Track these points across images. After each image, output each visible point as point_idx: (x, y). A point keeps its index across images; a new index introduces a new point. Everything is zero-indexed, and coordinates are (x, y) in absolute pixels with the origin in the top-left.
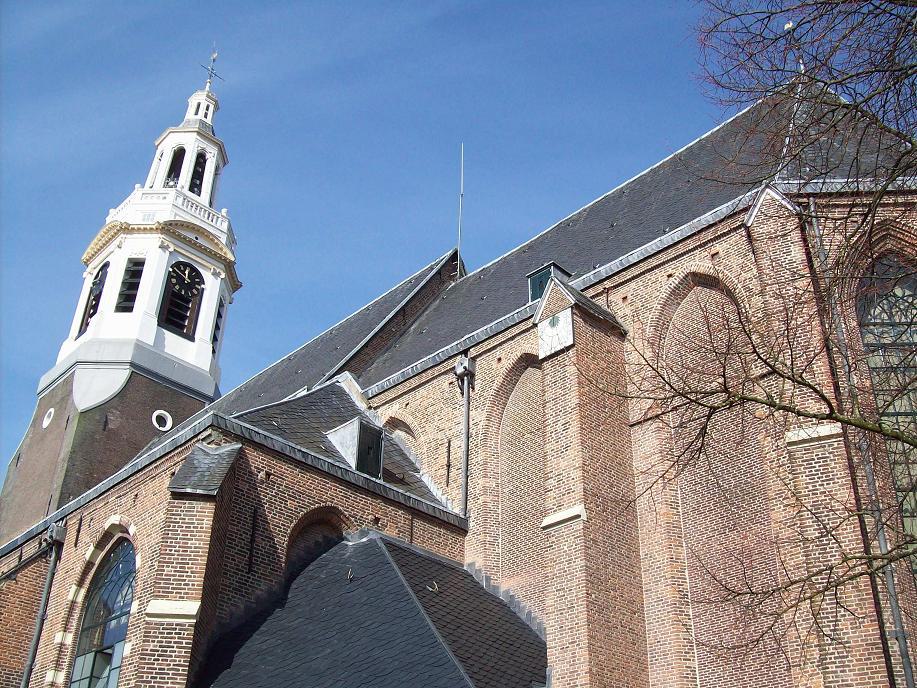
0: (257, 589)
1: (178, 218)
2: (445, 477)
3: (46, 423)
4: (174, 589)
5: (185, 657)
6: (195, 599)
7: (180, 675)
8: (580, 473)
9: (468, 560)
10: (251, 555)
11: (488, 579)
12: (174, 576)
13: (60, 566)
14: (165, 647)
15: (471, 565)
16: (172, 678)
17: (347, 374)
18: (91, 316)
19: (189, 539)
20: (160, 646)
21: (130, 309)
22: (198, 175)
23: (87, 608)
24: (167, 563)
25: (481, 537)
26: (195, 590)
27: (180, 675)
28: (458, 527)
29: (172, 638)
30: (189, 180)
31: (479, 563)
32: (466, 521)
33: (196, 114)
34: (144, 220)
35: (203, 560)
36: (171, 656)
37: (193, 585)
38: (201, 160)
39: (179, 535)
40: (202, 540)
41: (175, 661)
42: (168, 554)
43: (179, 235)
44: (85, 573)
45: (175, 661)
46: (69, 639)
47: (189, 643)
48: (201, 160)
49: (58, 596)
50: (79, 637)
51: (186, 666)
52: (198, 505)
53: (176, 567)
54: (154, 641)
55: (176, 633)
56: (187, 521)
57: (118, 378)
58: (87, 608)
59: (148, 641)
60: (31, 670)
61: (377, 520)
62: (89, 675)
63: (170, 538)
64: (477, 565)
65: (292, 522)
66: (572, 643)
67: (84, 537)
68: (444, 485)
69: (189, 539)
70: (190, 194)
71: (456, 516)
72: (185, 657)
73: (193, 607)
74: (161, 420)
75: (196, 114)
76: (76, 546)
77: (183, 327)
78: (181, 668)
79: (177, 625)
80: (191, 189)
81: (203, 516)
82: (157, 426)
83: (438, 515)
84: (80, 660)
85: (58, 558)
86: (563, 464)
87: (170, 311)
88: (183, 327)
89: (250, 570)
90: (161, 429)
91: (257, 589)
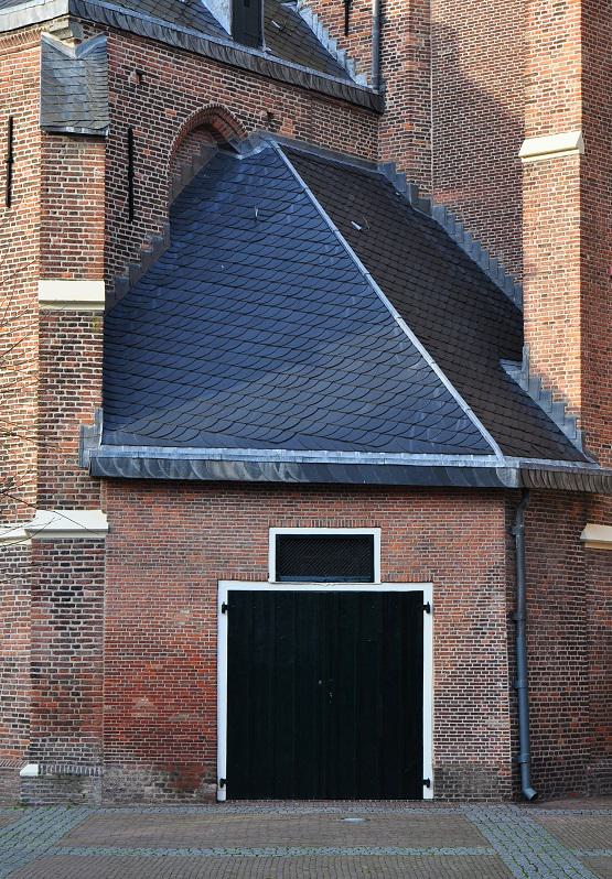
2: (341, 19)
4: (65, 264)
5: (97, 354)
7: (94, 377)
8: (578, 85)
9: (384, 159)
10: (131, 196)
11: (416, 190)
12: (64, 247)
15: (391, 166)
16: (84, 382)
19: (76, 197)
20: (63, 342)
24: (52, 230)
25: (405, 126)
26: (96, 265)
27: (94, 377)
28: (370, 107)
29: (77, 331)
31: (402, 164)
32: (381, 98)
37: (92, 259)
40: (94, 197)
41: (85, 360)
42: (52, 218)
45: (85, 360)
51: (99, 366)
52: (84, 149)
54: (54, 336)
55: (81, 325)
56: (69, 170)
59: (46, 336)
63: (51, 196)
64: (399, 167)
66: (559, 318)
69: (76, 197)
71: (368, 92)
72: (97, 354)
78: (94, 369)
81: (92, 165)
83: (346, 96)
86: (554, 66)
89: (132, 217)
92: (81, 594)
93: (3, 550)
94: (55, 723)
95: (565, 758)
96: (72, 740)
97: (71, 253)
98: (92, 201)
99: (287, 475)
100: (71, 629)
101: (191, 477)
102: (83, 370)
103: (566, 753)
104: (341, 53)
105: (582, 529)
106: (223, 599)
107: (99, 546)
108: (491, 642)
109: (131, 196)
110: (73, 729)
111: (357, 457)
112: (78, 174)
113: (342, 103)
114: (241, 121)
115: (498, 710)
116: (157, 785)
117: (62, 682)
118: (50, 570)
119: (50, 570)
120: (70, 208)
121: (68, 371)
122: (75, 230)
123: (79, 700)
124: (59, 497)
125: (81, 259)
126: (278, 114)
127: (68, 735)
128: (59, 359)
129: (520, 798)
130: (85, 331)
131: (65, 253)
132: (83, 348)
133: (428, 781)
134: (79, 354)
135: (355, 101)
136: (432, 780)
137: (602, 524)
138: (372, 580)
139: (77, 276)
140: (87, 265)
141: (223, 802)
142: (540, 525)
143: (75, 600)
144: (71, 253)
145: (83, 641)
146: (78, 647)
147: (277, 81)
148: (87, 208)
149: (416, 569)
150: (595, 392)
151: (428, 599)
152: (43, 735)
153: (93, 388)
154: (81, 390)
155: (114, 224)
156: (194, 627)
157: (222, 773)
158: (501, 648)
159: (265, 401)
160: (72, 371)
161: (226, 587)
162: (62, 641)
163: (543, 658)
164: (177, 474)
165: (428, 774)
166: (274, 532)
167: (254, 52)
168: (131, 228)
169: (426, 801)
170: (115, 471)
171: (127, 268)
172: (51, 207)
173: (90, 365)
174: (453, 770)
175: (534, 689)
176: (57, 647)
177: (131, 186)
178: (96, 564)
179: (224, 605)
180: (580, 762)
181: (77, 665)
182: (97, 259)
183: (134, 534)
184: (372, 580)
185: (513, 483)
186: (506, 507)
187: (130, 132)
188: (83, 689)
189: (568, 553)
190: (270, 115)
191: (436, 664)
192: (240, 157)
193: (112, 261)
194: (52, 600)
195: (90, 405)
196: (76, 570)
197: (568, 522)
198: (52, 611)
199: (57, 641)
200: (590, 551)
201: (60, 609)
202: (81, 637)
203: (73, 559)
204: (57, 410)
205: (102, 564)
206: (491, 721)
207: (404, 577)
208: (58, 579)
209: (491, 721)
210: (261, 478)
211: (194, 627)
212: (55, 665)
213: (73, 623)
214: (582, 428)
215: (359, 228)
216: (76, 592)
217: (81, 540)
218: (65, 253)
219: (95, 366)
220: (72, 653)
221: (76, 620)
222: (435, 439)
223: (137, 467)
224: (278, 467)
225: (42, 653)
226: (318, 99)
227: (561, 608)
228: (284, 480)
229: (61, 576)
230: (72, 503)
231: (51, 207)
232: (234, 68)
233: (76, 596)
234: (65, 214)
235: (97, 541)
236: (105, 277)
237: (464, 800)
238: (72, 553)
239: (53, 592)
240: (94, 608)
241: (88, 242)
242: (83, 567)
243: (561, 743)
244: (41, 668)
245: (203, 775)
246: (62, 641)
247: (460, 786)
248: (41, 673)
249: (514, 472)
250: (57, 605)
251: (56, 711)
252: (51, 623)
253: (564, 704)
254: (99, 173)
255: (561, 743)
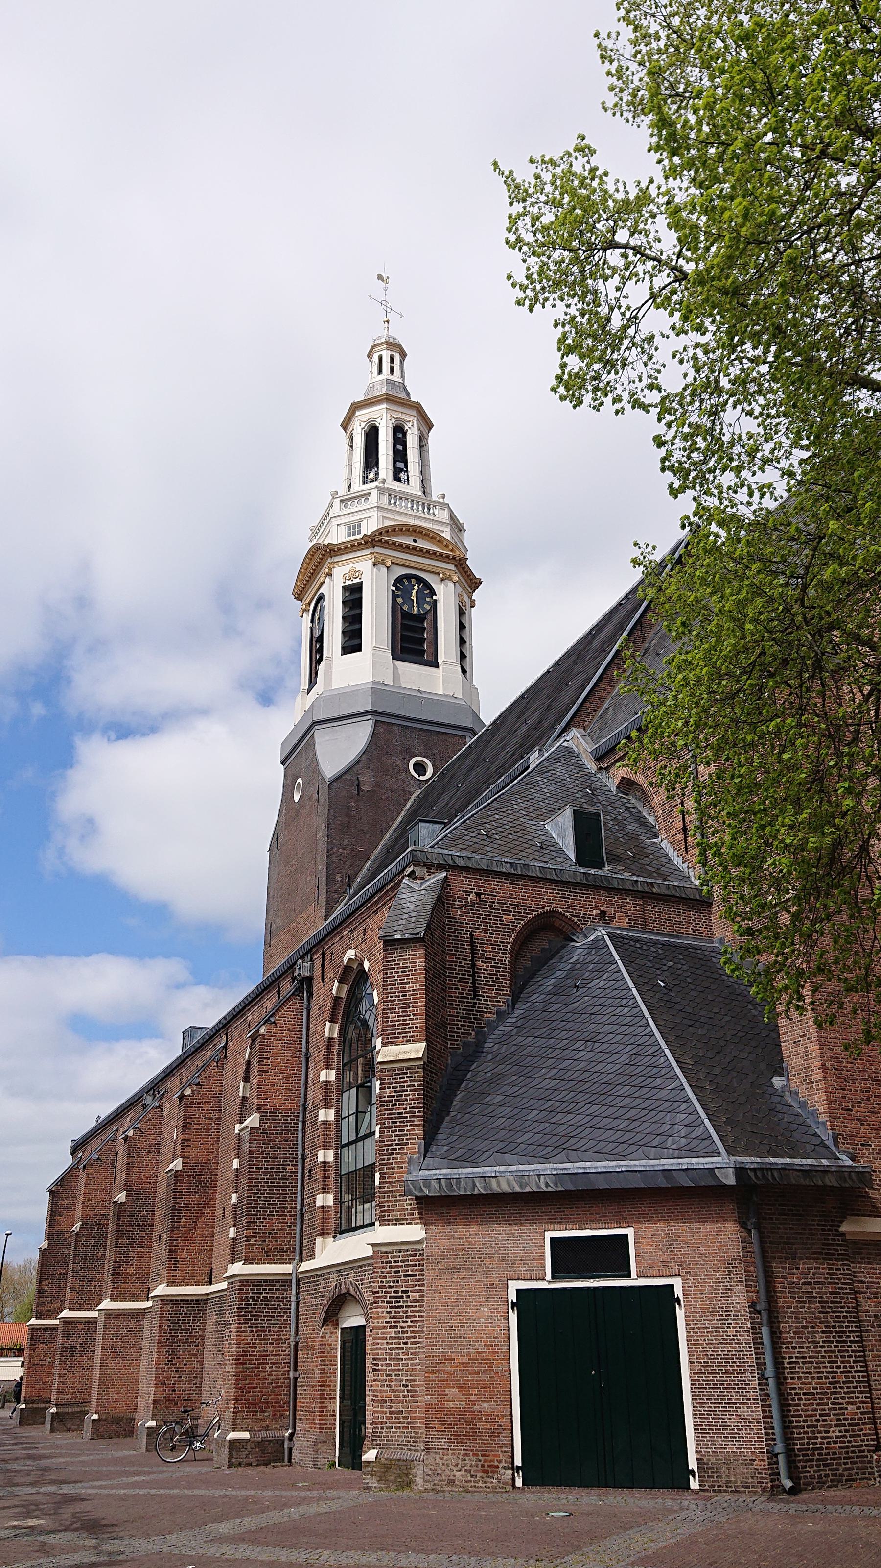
0: (485, 1012)
1: (388, 523)
3: (297, 798)
4: (399, 1033)
6: (420, 1041)
10: (474, 980)
13: (314, 1002)
14: (399, 1091)
16: (410, 1121)
17: (574, 732)
18: (319, 661)
19: (406, 983)
21: (358, 648)
22: (400, 455)
23: (344, 1042)
29: (405, 1082)
30: (391, 467)
33: (380, 371)
34: (349, 535)
35: (422, 1002)
36: (406, 1100)
37: (417, 1027)
38: (399, 433)
39: (396, 980)
43: (387, 542)
44: (334, 1009)
46: (332, 1075)
47: (420, 1085)
48: (399, 433)
49: (315, 1033)
50: (340, 1075)
51: (421, 1108)
53: (399, 1013)
54: (389, 1088)
55: (407, 1077)
57: (360, 734)
58: (344, 1042)
60: (305, 1109)
61: (603, 913)
62: (355, 1111)
63: (390, 985)
65: (510, 937)
67: (330, 974)
68: (682, 851)
69: (406, 983)
70: (396, 486)
72: (418, 1099)
73: (416, 1050)
74: (420, 768)
75: (380, 371)
76: (323, 981)
77: (423, 652)
79: (407, 1069)
80: (397, 478)
82: (416, 776)
84: (346, 1095)
85: (311, 995)
87: (404, 638)
88: (423, 652)
90: (422, 778)
91: (485, 1012)
92: (408, 1297)
93: (879, 1293)
94: (391, 1412)
95: (840, 1448)
96: (403, 1428)
97: (403, 1024)
98: (416, 984)
99: (547, 1185)
100: (401, 1327)
101: (476, 1192)
102: (410, 1112)
103: (841, 1442)
104: (685, 865)
105: (842, 1222)
106: (513, 1297)
107: (421, 1255)
108: (737, 1332)
109: (474, 980)
110: (404, 1417)
111: (602, 1166)
112: (407, 967)
113: (673, 899)
114: (576, 919)
115: (749, 1400)
116: (465, 1471)
117: (395, 1375)
118: (385, 1277)
119: (385, 1277)
120: (402, 992)
121: (398, 1113)
122: (405, 1008)
123: (408, 1391)
124: (395, 1215)
125: (410, 1028)
126: (611, 911)
127: (400, 1423)
128: (393, 1105)
129: (775, 1490)
130: (411, 1081)
131: (399, 1025)
132: (409, 1095)
133: (693, 1471)
134: (406, 1100)
135: (684, 896)
136: (696, 1470)
137: (869, 1216)
138: (628, 1276)
139: (407, 1041)
140: (413, 1032)
141: (519, 1488)
142: (786, 1219)
143: (404, 1302)
144: (403, 1024)
145: (410, 1338)
146: (406, 1343)
147: (608, 889)
148: (413, 990)
149: (665, 1264)
150: (844, 1097)
151: (678, 1292)
152: (382, 1423)
153: (416, 1125)
154: (409, 1128)
155: (459, 1001)
156: (491, 1323)
157: (518, 1462)
158: (746, 1338)
159: (690, 1140)
160: (402, 1113)
161: (514, 1286)
162: (395, 1338)
163: (802, 1347)
164: (465, 1190)
165: (693, 1464)
166: (549, 1235)
167: (600, 872)
168: (475, 1003)
169: (692, 1491)
170: (421, 1190)
171: (473, 1033)
172: (389, 993)
173: (413, 1108)
174: (713, 1460)
175: (793, 1378)
176: (391, 1344)
177: (474, 972)
178: (418, 1270)
179: (512, 1303)
180: (863, 1451)
181: (406, 1359)
182: (421, 1027)
183: (445, 1243)
184: (628, 1276)
185: (731, 1181)
186: (737, 1203)
187: (472, 935)
188: (411, 1381)
189: (824, 1244)
190: (603, 913)
191: (690, 1354)
192: (577, 944)
193: (460, 1029)
194: (388, 1303)
195: (414, 1139)
196: (405, 1276)
197: (820, 1216)
198: (388, 1312)
199: (391, 1338)
200: (855, 1242)
201: (393, 1310)
202: (409, 1334)
203: (402, 1266)
204: (392, 1145)
205: (423, 1270)
206: (744, 1411)
207: (655, 1272)
208: (392, 1284)
209: (744, 1411)
210: (528, 1189)
211: (491, 1323)
212: (390, 1359)
213: (403, 1322)
214: (832, 1129)
215: (662, 985)
216: (404, 1295)
217: (408, 1250)
218: (399, 1025)
219: (417, 1108)
220: (402, 1348)
221: (405, 1319)
222: (673, 1147)
223: (437, 1186)
224: (539, 1179)
225: (380, 1349)
226: (648, 898)
227: (821, 1297)
228: (545, 1189)
229: (394, 1282)
230: (403, 1219)
231: (389, 993)
232: (565, 883)
233: (405, 1299)
234: (399, 996)
235: (419, 1250)
236: (427, 1040)
237: (726, 1491)
238: (402, 1261)
239: (388, 1295)
240: (418, 1309)
241: (414, 1015)
242: (410, 1273)
243: (835, 1432)
244: (380, 1363)
245: (500, 1461)
246: (395, 1338)
247: (721, 1477)
248: (380, 1367)
249: (731, 1170)
250: (391, 1307)
251: (391, 1401)
252: (386, 1322)
253: (835, 1393)
254: (420, 964)
255: (835, 1432)
